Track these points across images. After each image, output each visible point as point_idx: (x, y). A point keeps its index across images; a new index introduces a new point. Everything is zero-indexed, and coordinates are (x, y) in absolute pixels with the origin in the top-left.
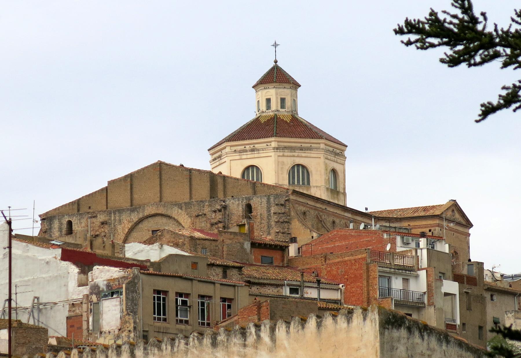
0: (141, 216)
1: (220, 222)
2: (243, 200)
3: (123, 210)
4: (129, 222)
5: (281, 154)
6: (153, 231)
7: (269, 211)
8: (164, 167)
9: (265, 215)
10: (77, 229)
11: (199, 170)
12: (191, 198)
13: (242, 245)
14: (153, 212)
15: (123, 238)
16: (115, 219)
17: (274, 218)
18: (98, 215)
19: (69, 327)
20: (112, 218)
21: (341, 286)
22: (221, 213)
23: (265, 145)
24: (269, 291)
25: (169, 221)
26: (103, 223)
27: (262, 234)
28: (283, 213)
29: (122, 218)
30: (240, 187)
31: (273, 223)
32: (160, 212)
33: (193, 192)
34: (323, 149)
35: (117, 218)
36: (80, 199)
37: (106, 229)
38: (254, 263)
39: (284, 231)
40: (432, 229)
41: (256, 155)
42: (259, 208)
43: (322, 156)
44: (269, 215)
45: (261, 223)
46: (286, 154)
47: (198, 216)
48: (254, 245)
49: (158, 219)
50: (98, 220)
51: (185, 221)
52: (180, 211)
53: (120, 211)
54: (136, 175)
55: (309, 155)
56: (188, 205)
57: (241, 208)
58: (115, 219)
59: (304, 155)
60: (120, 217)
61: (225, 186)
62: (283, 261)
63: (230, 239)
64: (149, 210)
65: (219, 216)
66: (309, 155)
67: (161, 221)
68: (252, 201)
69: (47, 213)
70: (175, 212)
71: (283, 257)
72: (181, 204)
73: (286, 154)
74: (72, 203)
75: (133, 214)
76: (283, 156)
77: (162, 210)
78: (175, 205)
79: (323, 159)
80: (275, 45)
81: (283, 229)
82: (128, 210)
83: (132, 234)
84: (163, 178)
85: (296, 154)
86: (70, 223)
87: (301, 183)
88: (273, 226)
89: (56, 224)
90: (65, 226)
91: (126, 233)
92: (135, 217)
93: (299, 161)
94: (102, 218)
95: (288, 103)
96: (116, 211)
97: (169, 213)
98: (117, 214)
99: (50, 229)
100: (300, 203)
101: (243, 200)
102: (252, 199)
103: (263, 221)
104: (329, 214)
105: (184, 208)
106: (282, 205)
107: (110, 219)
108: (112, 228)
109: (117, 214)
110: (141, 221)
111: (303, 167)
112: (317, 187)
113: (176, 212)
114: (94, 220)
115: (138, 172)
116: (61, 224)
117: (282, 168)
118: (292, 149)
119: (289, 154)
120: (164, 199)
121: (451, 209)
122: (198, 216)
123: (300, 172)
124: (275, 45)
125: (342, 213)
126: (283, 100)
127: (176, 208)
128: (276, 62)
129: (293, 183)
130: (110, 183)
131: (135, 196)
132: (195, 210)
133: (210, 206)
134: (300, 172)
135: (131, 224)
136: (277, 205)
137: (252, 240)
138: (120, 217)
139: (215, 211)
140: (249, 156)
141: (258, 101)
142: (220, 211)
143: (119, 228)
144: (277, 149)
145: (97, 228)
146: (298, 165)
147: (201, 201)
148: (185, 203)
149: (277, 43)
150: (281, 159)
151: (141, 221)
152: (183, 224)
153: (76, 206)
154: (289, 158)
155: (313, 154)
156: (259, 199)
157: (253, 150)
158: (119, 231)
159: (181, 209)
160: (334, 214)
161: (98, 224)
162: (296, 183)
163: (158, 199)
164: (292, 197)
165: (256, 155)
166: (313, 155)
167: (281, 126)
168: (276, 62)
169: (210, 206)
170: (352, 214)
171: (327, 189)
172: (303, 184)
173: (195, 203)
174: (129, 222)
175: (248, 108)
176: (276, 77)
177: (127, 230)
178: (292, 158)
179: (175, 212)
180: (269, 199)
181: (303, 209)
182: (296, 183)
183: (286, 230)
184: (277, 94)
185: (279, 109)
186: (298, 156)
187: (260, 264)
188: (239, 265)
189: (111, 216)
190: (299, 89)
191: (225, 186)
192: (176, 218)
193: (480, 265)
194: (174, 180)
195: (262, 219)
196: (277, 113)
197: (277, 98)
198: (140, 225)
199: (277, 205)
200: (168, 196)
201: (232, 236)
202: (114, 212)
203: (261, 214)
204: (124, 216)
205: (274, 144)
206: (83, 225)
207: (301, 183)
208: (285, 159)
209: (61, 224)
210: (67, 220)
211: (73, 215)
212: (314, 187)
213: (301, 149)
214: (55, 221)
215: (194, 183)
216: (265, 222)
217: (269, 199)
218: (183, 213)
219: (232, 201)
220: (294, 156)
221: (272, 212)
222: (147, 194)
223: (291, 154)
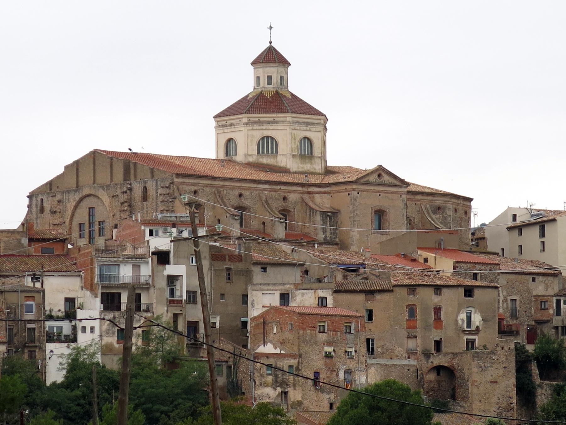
1: (126, 202)
3: (70, 191)
4: (74, 201)
5: (251, 128)
6: (90, 208)
8: (97, 155)
9: (155, 196)
12: (112, 180)
13: (19, 241)
17: (160, 198)
21: (82, 273)
22: (126, 194)
23: (238, 120)
24: (11, 281)
28: (168, 194)
31: (159, 203)
32: (91, 193)
33: (114, 176)
34: (289, 122)
36: (52, 180)
38: (34, 254)
39: (168, 209)
40: (350, 193)
41: (233, 130)
43: (288, 128)
44: (157, 196)
46: (255, 128)
48: (31, 240)
53: (68, 192)
55: (276, 128)
59: (271, 128)
61: (135, 171)
62: (63, 250)
63: (7, 237)
64: (86, 191)
66: (276, 128)
69: (33, 191)
71: (64, 247)
72: (104, 187)
73: (255, 128)
74: (47, 184)
76: (253, 130)
79: (289, 131)
80: (271, 28)
81: (168, 207)
84: (96, 164)
85: (264, 127)
86: (42, 200)
87: (270, 152)
92: (77, 197)
93: (267, 133)
94: (58, 197)
95: (275, 80)
97: (97, 194)
98: (67, 194)
100: (188, 184)
104: (232, 188)
106: (167, 187)
107: (63, 198)
109: (67, 194)
110: (81, 200)
111: (272, 139)
112: (283, 155)
114: (54, 198)
116: (37, 201)
117: (252, 140)
118: (260, 123)
119: (258, 128)
120: (97, 182)
121: (377, 173)
123: (268, 144)
124: (271, 28)
125: (255, 186)
126: (269, 78)
128: (271, 43)
129: (263, 152)
131: (80, 179)
133: (121, 188)
134: (268, 144)
136: (162, 187)
137: (31, 236)
140: (229, 130)
141: (258, 78)
142: (126, 192)
143: (68, 205)
144: (247, 124)
146: (268, 137)
148: (107, 186)
149: (272, 26)
150: (250, 133)
151: (81, 200)
153: (48, 186)
154: (257, 131)
155: (280, 126)
157: (231, 125)
159: (104, 190)
160: (240, 188)
162: (265, 152)
163: (92, 182)
164: (176, 180)
165: (233, 130)
166: (279, 128)
167: (272, 101)
168: (271, 43)
170: (269, 185)
171: (294, 156)
172: (272, 152)
174: (74, 201)
175: (244, 84)
176: (271, 57)
178: (261, 131)
180: (157, 183)
181: (193, 188)
182: (265, 152)
183: (170, 208)
184: (264, 72)
185: (267, 86)
186: (266, 129)
187: (40, 254)
188: (308, 211)
190: (290, 68)
191: (135, 171)
195: (153, 199)
196: (263, 89)
197: (264, 76)
198: (82, 204)
199: (162, 187)
201: (10, 234)
205: (245, 120)
206: (50, 202)
207: (270, 152)
208: (254, 133)
209: (37, 201)
212: (280, 155)
213: (269, 123)
215: (114, 168)
217: (157, 183)
218: (105, 193)
220: (262, 129)
223: (260, 128)
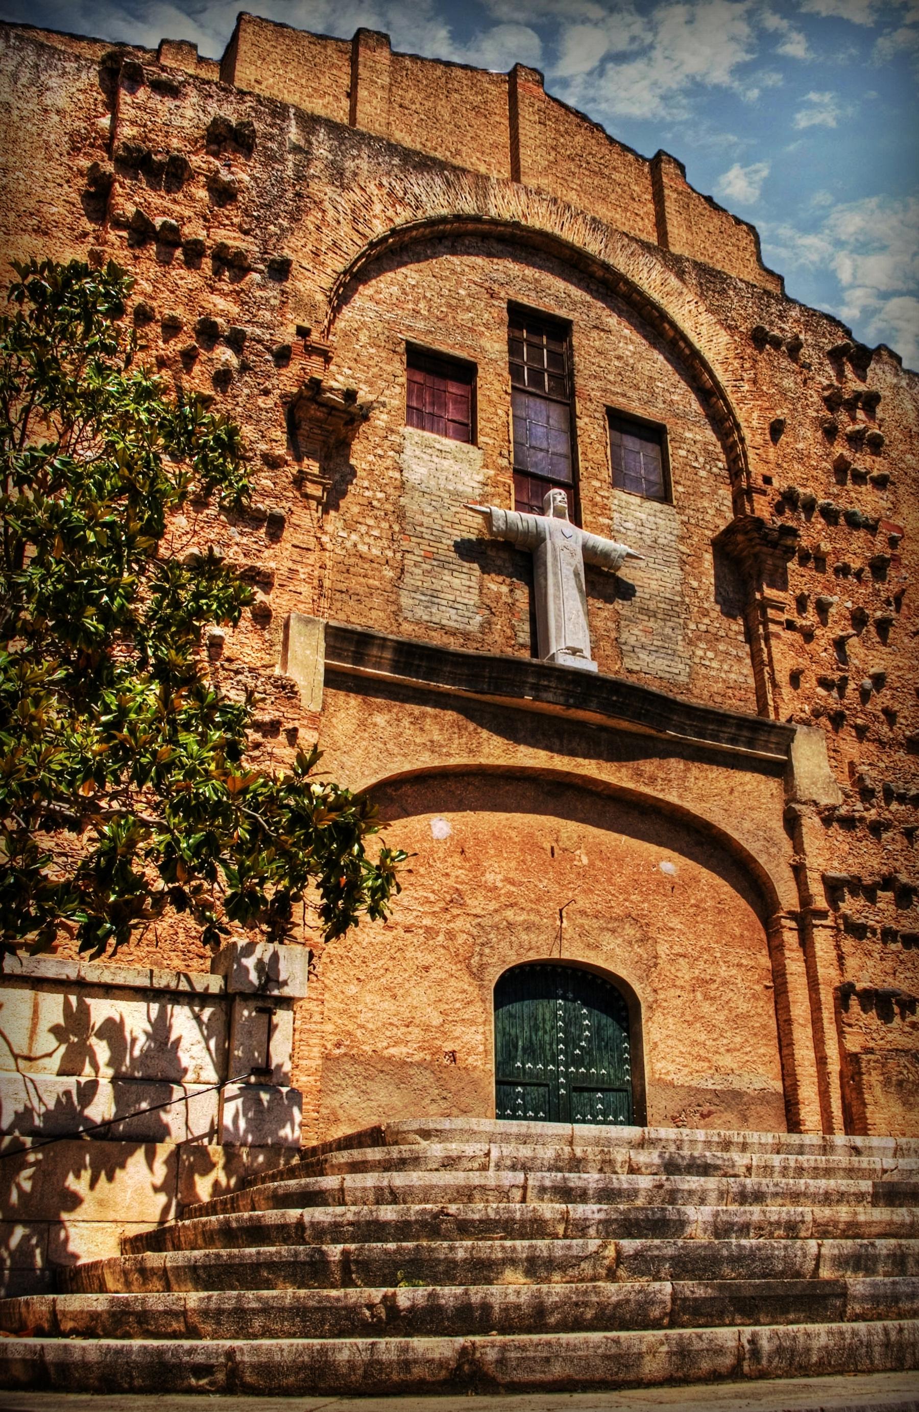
52: (674, 281)
91: (373, 237)
92: (436, 200)
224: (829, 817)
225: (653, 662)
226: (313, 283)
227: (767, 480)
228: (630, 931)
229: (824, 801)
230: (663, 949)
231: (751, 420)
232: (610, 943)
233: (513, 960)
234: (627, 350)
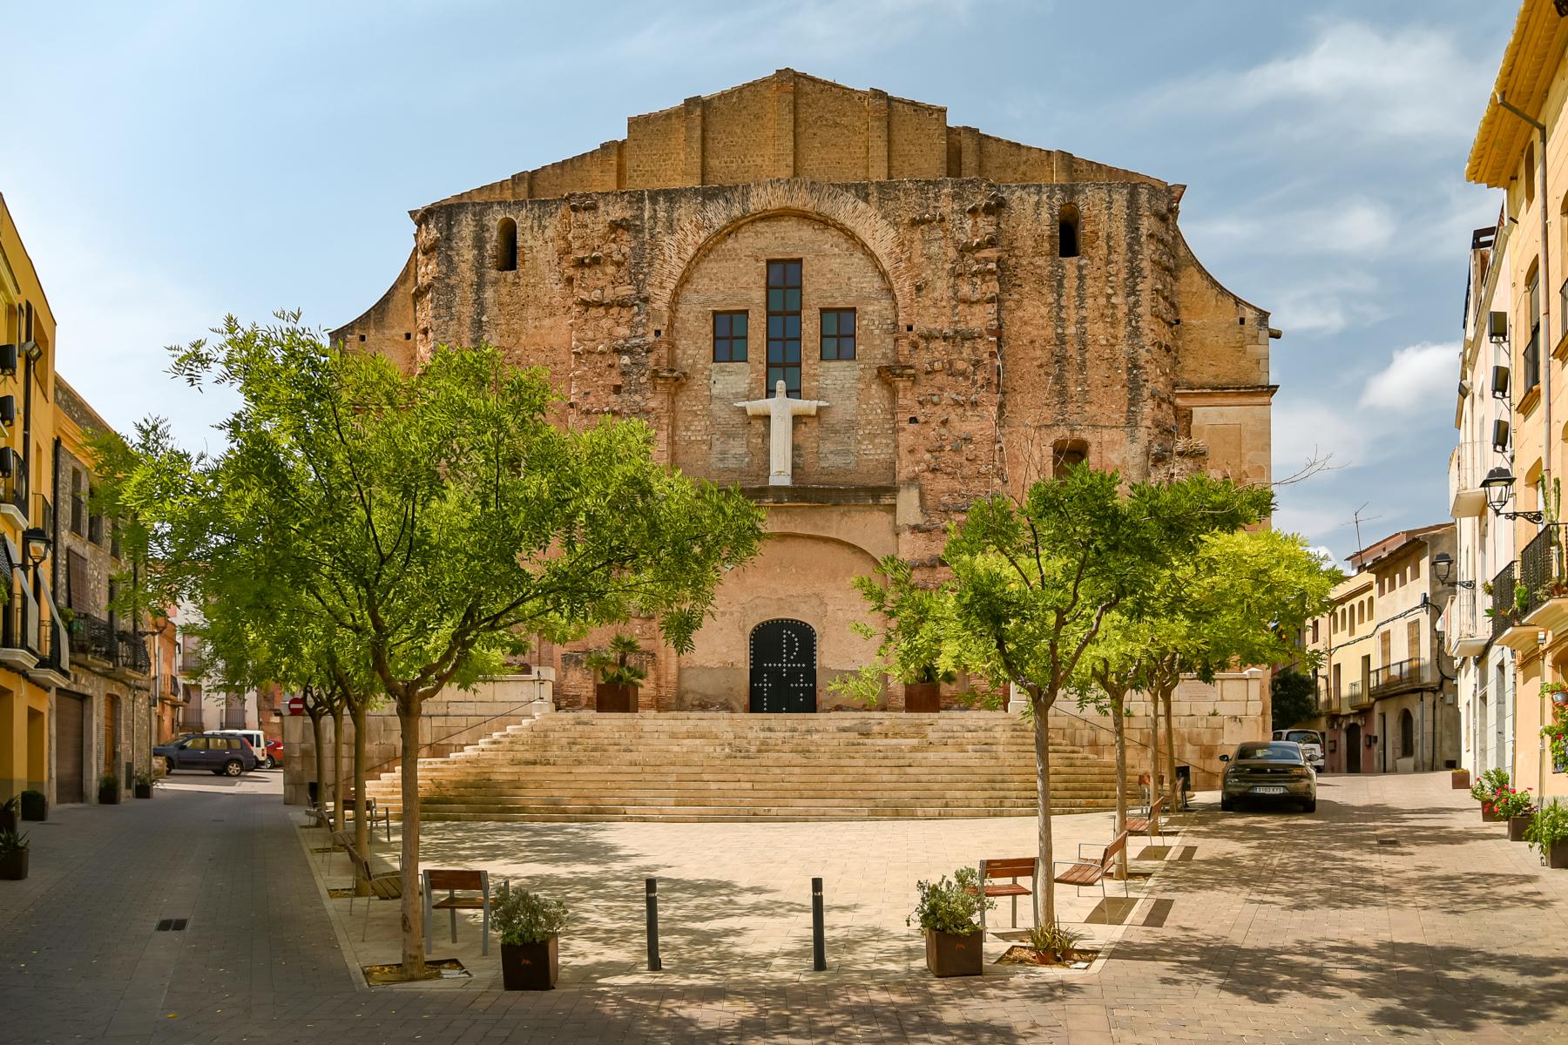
0: (737, 211)
2: (1052, 191)
4: (699, 227)
7: (1133, 228)
10: (530, 243)
11: (913, 103)
14: (775, 205)
15: (678, 272)
16: (654, 217)
18: (601, 204)
19: (1409, 762)
20: (646, 215)
25: (820, 237)
26: (616, 226)
27: (1110, 291)
29: (676, 215)
30: (1023, 168)
31: (1146, 265)
32: (797, 204)
35: (661, 214)
37: (625, 245)
42: (1104, 218)
45: (1109, 262)
47: (915, 223)
49: (789, 228)
50: (601, 219)
51: (878, 235)
52: (861, 205)
54: (716, 103)
56: (887, 190)
57: (1045, 216)
58: (654, 217)
60: (670, 211)
65: (986, 226)
67: (797, 234)
68: (1082, 197)
70: (847, 210)
72: (866, 186)
75: (711, 207)
77: (802, 200)
78: (847, 187)
82: (696, 192)
83: (703, 265)
86: (509, 232)
88: (1147, 272)
89: (466, 228)
90: (493, 236)
91: (688, 258)
96: (658, 193)
97: (826, 207)
98: (662, 204)
99: (448, 239)
101: (1052, 191)
102: (1083, 191)
103: (1114, 257)
105: (874, 198)
107: (640, 217)
108: (644, 243)
109: (662, 204)
110: (733, 228)
113: (849, 207)
114: (586, 217)
115: (723, 96)
116: (482, 228)
122: (915, 223)
127: (850, 197)
130: (635, 123)
132: (909, 207)
135: (704, 234)
138: (670, 211)
139: (973, 211)
145: (596, 243)
147: (928, 182)
148: (880, 185)
152: (870, 243)
156: (1103, 194)
158: (667, 252)
159: (866, 199)
161: (601, 228)
169: (955, 197)
173: (909, 185)
174: (699, 227)
177: (691, 251)
179: (847, 210)
189: (642, 209)
192: (849, 224)
193: (183, 458)
194: (836, 125)
200: (814, 161)
202: (651, 198)
203: (1109, 237)
204: (682, 211)
210: (499, 217)
211: (519, 204)
214: (462, 216)
215: (900, 137)
216: (1120, 256)
218: (872, 211)
219: (1018, 194)
221: (1144, 231)
222: (762, 158)
224: (916, 529)
225: (831, 459)
226: (661, 301)
227: (910, 328)
228: (815, 601)
229: (913, 523)
230: (830, 608)
231: (904, 287)
232: (804, 608)
233: (758, 621)
234: (835, 264)
